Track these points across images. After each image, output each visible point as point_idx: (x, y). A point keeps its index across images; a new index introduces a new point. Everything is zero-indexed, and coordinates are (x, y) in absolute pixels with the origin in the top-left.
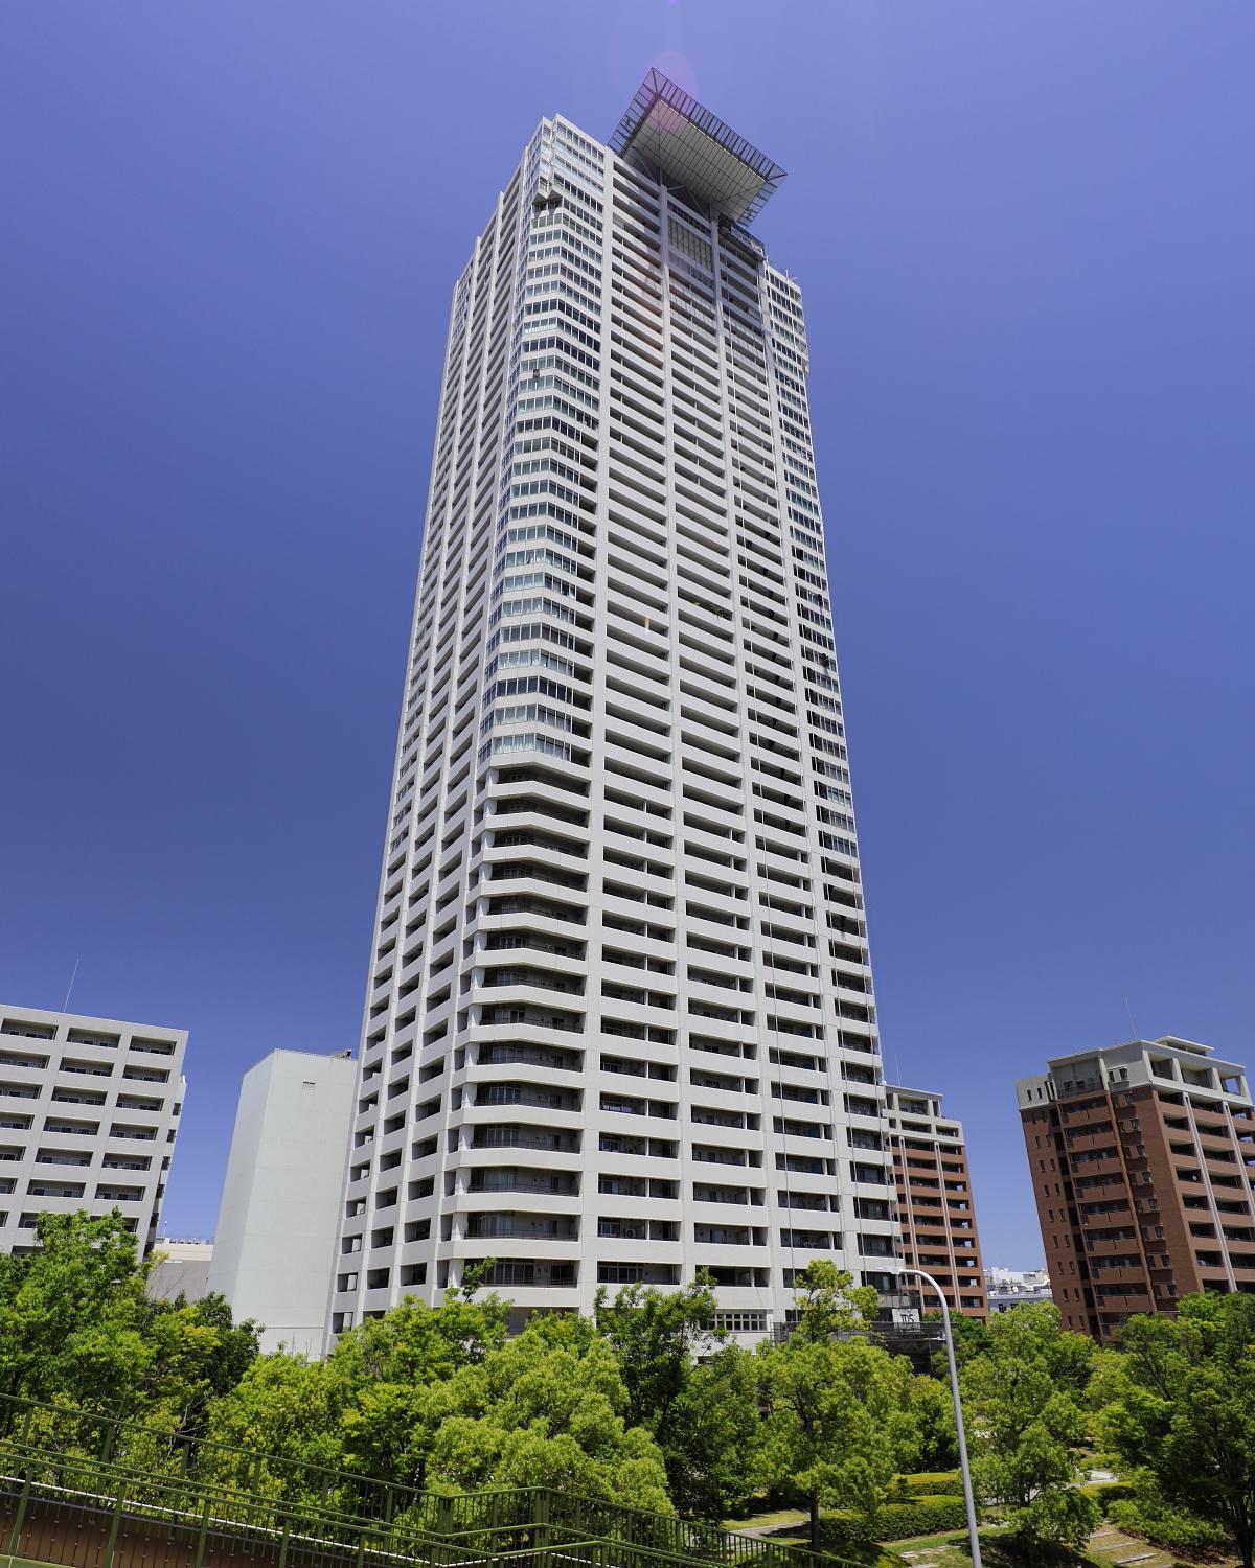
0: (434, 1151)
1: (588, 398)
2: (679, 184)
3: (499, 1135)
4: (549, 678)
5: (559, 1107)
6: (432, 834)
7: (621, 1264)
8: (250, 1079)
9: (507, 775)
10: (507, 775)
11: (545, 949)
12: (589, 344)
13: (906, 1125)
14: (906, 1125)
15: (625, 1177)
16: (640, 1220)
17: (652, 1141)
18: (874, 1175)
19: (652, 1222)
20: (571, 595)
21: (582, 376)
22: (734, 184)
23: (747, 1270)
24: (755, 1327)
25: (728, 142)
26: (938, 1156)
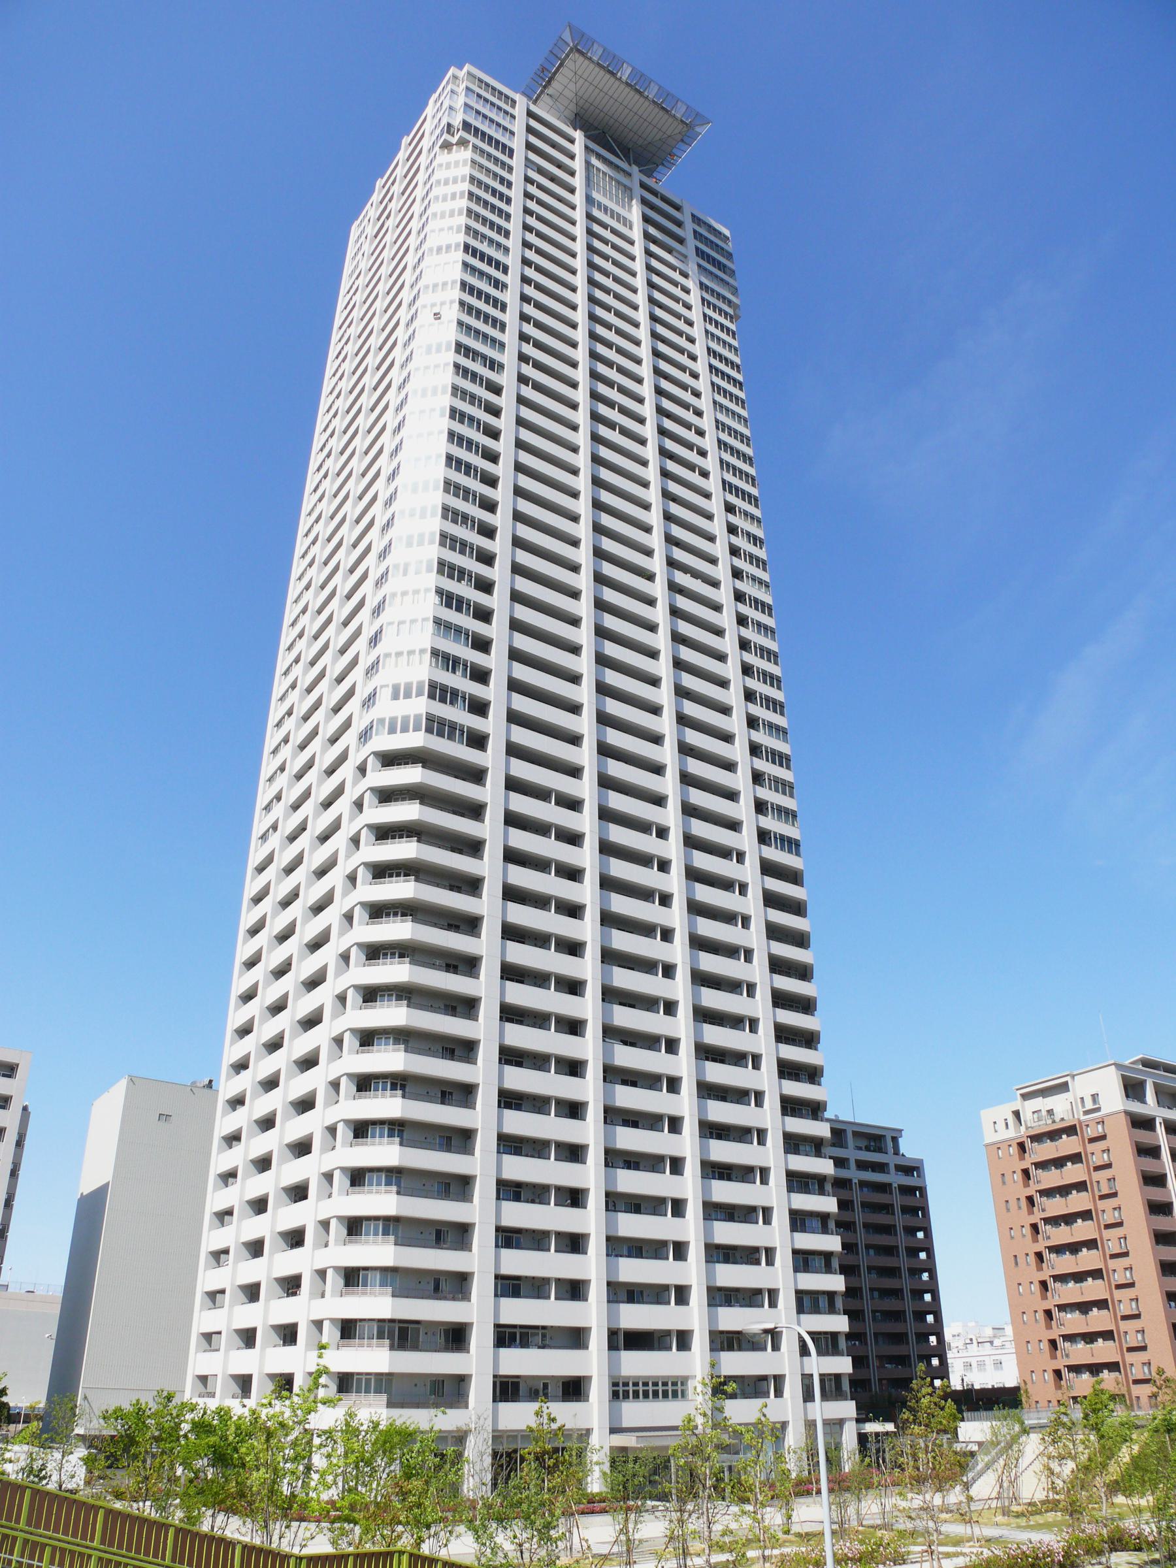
0: (305, 1197)
1: (494, 340)
2: (596, 128)
3: (368, 1227)
4: (448, 718)
5: (449, 1151)
6: (304, 829)
7: (522, 1327)
8: (97, 1103)
9: (390, 759)
10: (390, 759)
11: (433, 966)
12: (499, 232)
13: (862, 1165)
14: (862, 1165)
15: (527, 1230)
16: (543, 1279)
17: (559, 1189)
18: (816, 1223)
19: (558, 1280)
20: (459, 673)
21: (487, 318)
22: (651, 127)
23: (668, 1333)
24: (675, 1394)
25: (372, 1008)
26: (897, 1200)
